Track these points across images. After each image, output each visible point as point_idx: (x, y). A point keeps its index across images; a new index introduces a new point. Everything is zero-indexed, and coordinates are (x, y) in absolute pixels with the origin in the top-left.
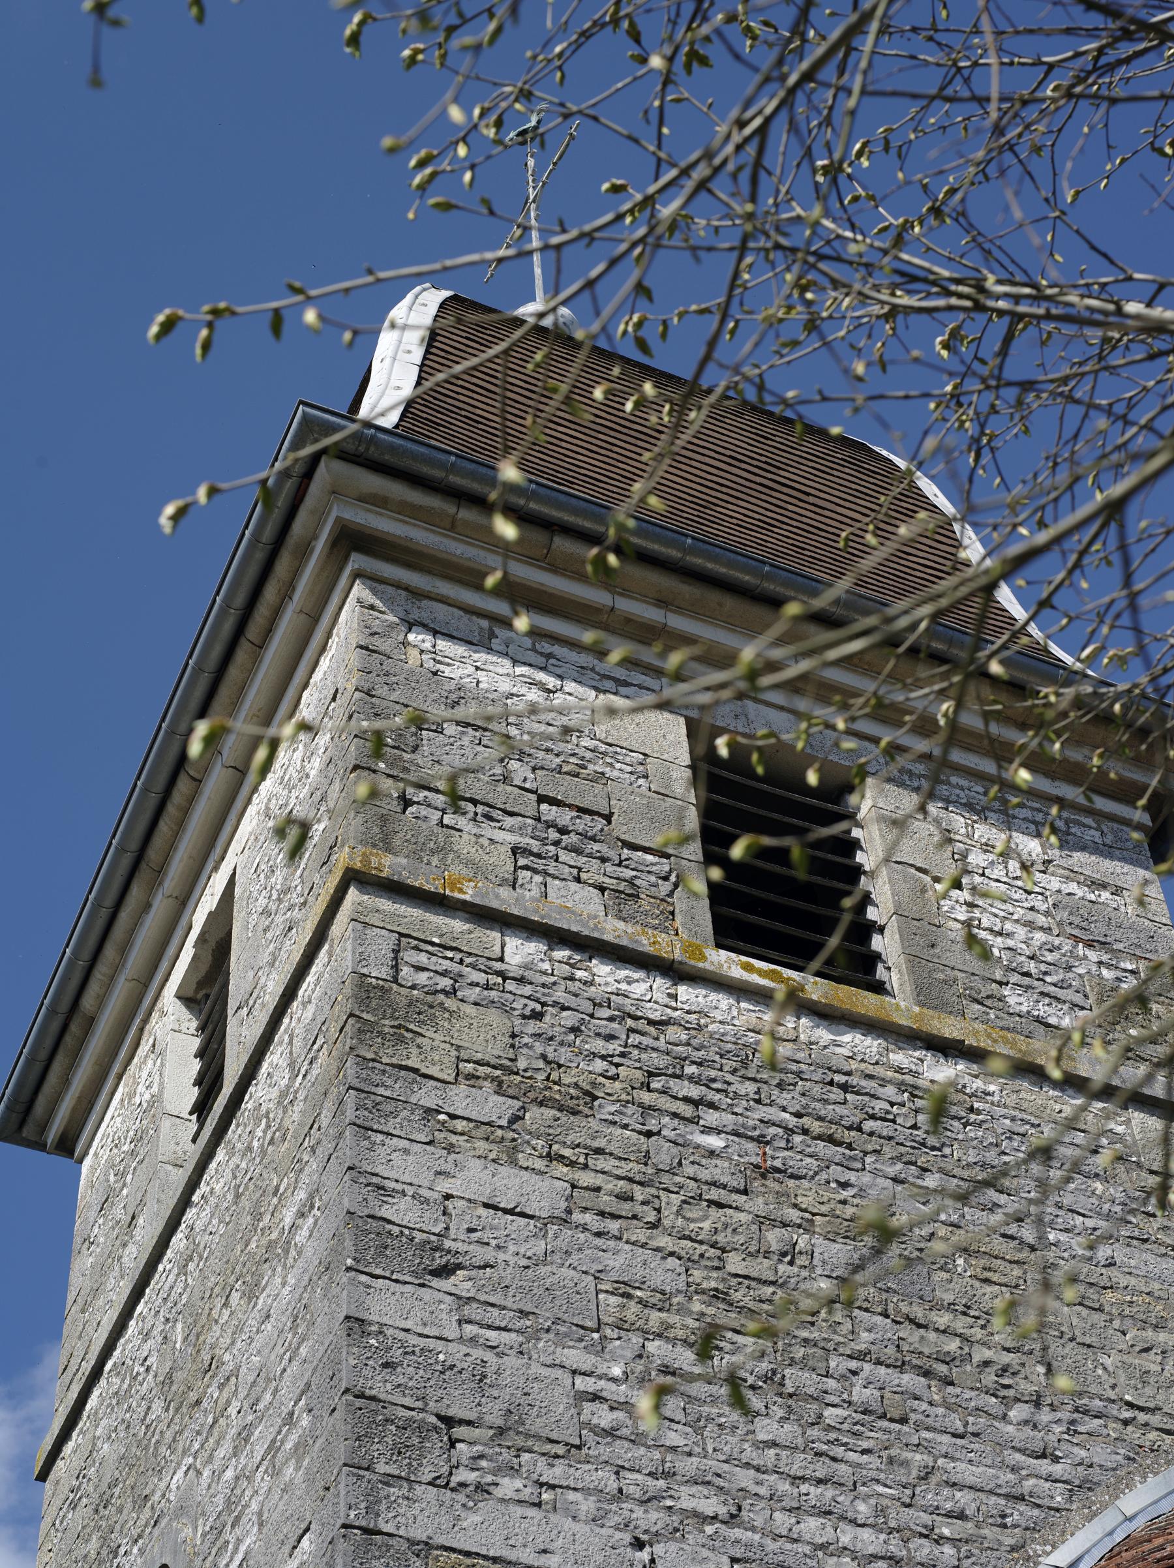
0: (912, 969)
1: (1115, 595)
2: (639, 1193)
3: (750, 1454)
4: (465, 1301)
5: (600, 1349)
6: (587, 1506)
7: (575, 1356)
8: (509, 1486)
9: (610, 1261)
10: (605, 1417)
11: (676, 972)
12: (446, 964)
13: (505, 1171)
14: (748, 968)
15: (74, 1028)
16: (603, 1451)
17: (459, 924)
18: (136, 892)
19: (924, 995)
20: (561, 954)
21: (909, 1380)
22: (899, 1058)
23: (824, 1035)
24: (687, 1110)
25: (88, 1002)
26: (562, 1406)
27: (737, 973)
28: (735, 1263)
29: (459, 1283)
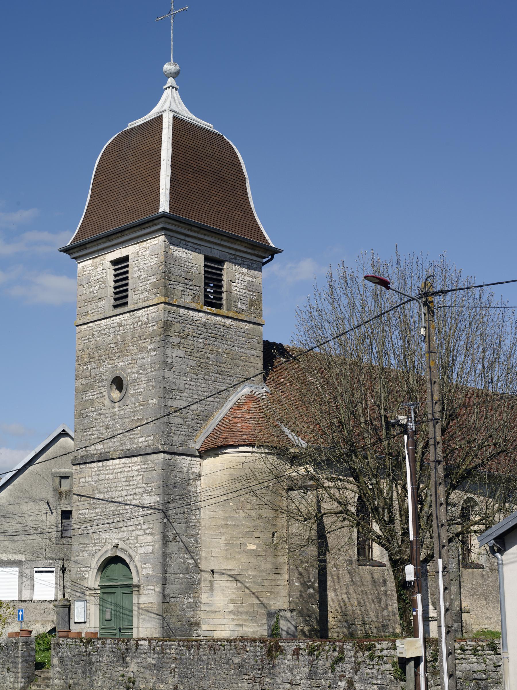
0: (227, 302)
1: (296, 593)
2: (192, 351)
3: (201, 389)
4: (174, 372)
5: (187, 377)
6: (185, 399)
7: (185, 378)
8: (178, 397)
9: (189, 363)
10: (187, 386)
11: (199, 311)
12: (173, 316)
13: (179, 351)
14: (208, 309)
15: (83, 247)
16: (186, 391)
17: (175, 308)
18: (104, 240)
19: (228, 310)
20: (186, 310)
21: (218, 375)
22: (223, 320)
23: (215, 318)
24: (198, 336)
25: (88, 246)
26: (183, 384)
27: (206, 310)
28: (202, 361)
29: (173, 369)
